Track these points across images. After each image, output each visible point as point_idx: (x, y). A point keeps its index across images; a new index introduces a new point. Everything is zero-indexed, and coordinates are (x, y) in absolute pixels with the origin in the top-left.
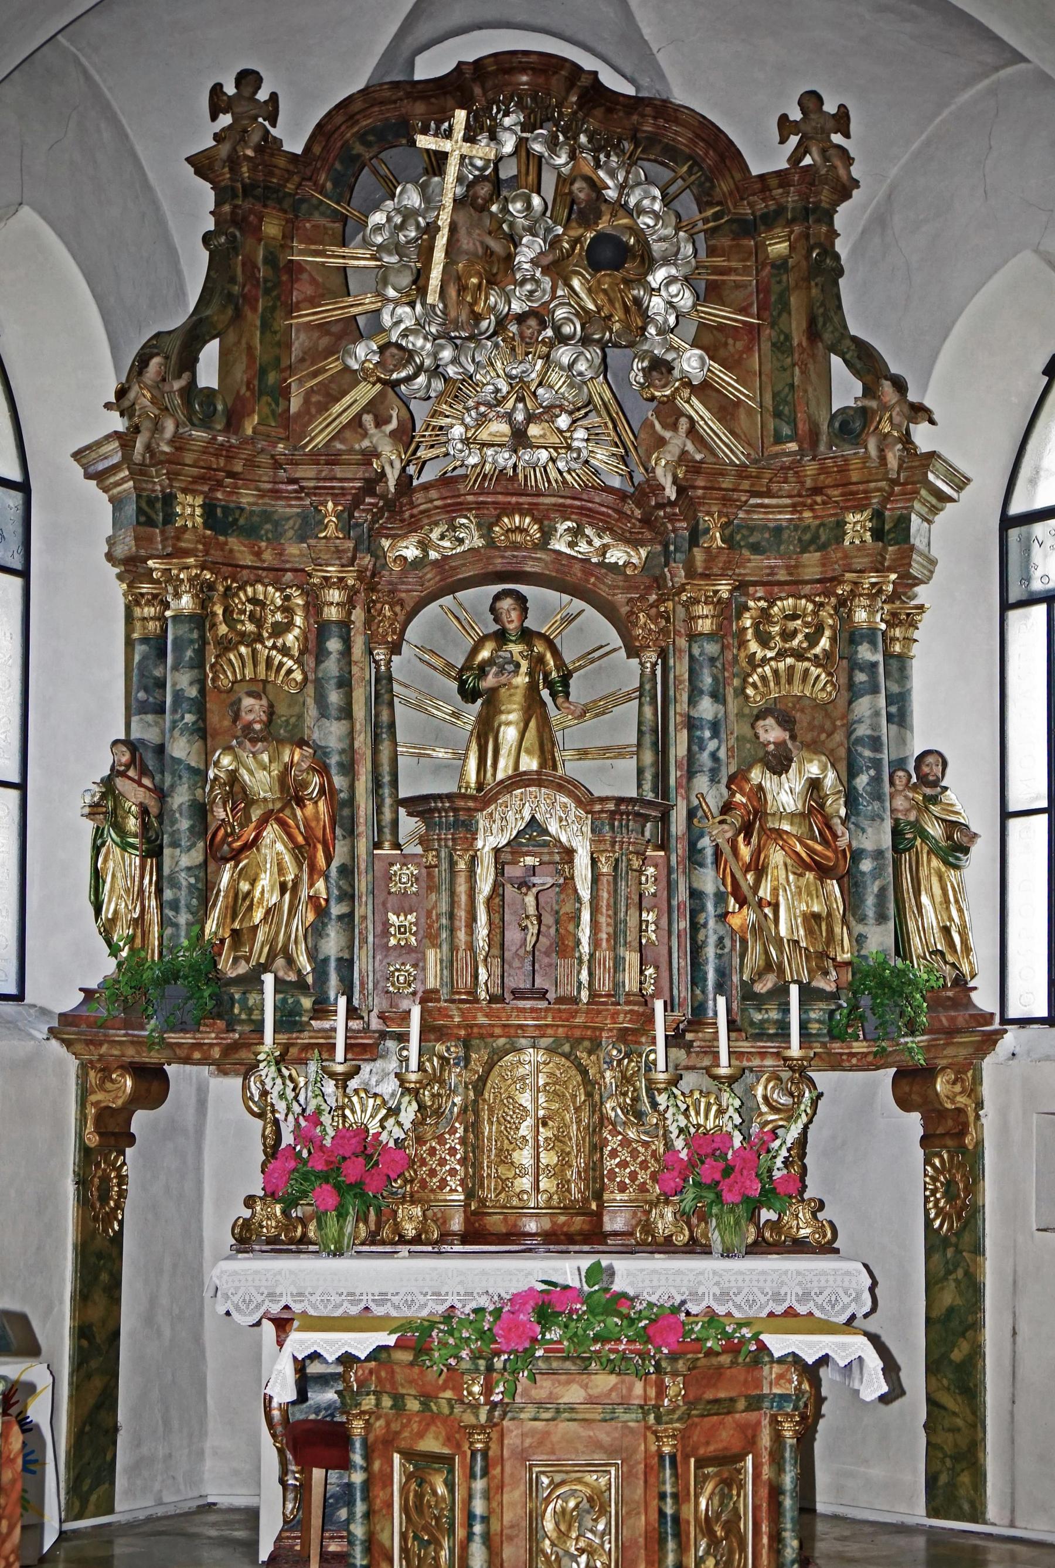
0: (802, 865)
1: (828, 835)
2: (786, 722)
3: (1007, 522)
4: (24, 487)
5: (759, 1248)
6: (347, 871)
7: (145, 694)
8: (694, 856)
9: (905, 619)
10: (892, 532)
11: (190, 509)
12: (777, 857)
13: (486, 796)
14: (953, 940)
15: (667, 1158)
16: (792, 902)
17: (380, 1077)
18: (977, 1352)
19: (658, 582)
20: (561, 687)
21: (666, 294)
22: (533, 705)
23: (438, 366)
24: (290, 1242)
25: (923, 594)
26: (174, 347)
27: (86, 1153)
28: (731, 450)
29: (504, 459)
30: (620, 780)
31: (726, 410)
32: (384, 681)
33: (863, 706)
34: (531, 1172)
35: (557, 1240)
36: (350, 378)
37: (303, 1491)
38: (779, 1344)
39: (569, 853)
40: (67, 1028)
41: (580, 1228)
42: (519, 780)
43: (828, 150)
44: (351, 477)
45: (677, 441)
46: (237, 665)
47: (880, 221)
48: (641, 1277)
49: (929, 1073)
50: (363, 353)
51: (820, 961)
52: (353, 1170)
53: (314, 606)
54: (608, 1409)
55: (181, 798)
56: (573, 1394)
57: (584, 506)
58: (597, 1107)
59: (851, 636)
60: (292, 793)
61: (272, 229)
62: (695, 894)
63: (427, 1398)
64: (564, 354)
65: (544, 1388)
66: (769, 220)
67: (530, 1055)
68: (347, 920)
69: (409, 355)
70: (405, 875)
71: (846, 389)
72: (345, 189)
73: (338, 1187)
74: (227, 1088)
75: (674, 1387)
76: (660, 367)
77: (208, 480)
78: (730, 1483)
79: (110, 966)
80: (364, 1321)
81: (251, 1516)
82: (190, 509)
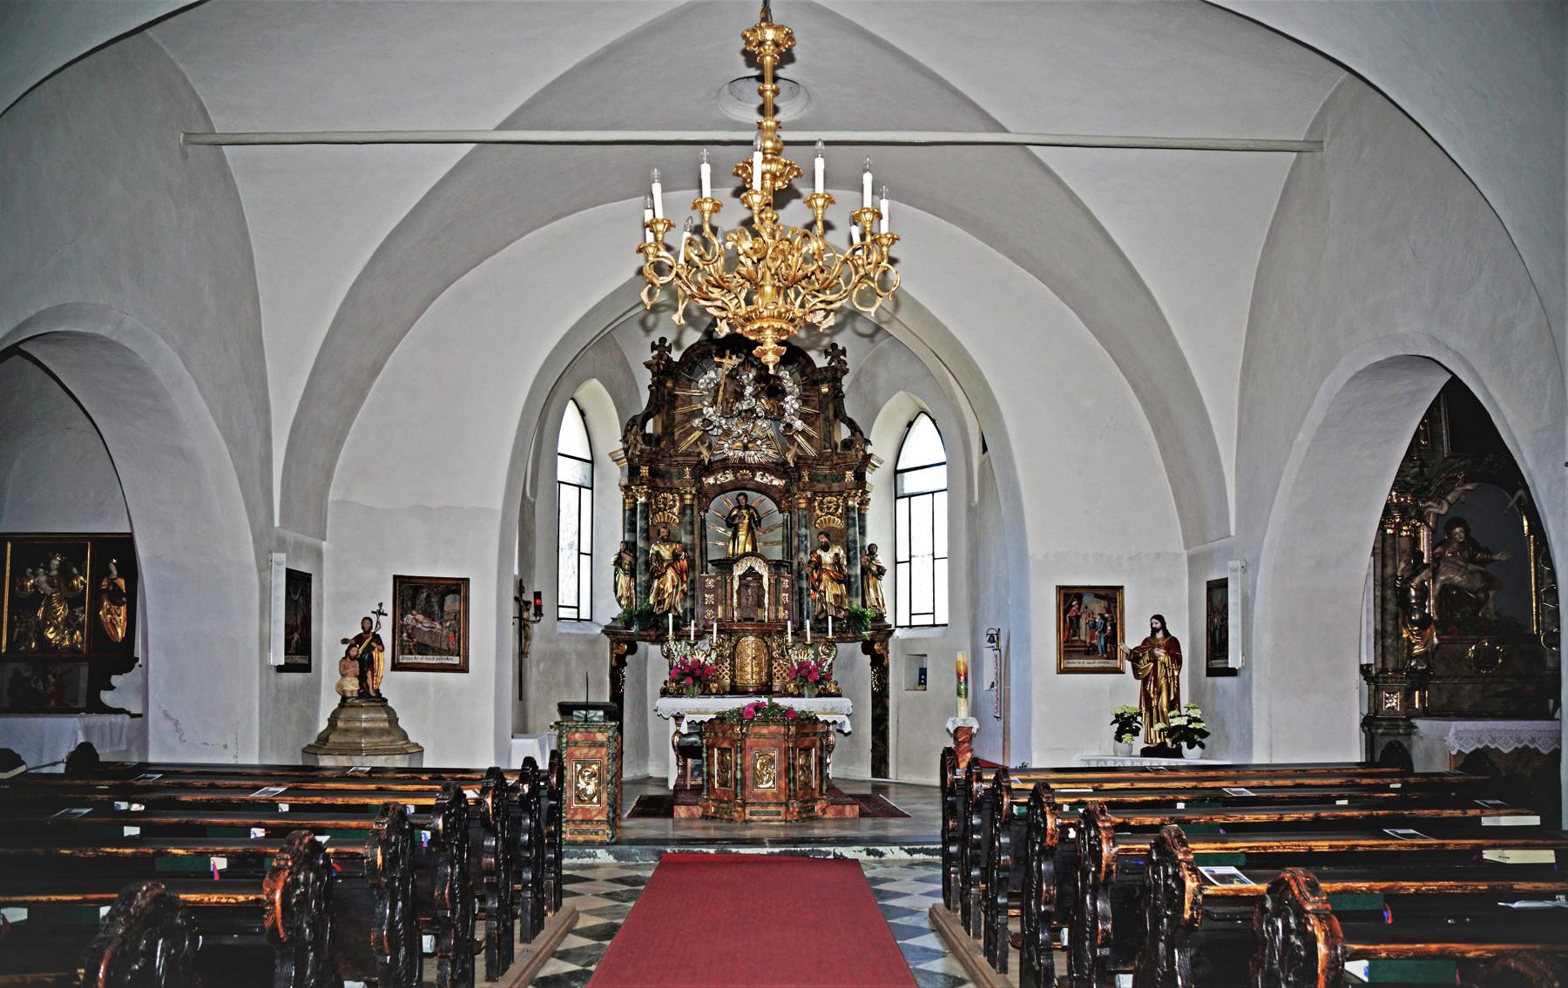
0: (833, 580)
1: (841, 571)
2: (827, 536)
3: (897, 472)
4: (592, 462)
5: (819, 695)
6: (693, 582)
7: (630, 526)
8: (800, 577)
9: (864, 503)
10: (860, 478)
11: (645, 471)
12: (824, 577)
13: (737, 559)
14: (880, 605)
15: (792, 669)
16: (831, 590)
17: (704, 645)
18: (887, 727)
19: (788, 491)
20: (758, 523)
21: (791, 403)
22: (750, 529)
23: (883, 789)
24: (679, 694)
25: (870, 496)
26: (639, 421)
27: (612, 667)
28: (811, 452)
29: (740, 454)
30: (777, 553)
31: (809, 439)
32: (703, 522)
33: (851, 531)
34: (750, 675)
35: (758, 693)
36: (693, 429)
37: (684, 767)
38: (821, 718)
39: (761, 577)
40: (608, 631)
41: (765, 689)
42: (746, 554)
43: (840, 361)
44: (694, 460)
45: (794, 450)
46: (659, 517)
47: (857, 379)
48: (783, 702)
49: (872, 642)
50: (697, 422)
51: (838, 608)
52: (698, 672)
53: (682, 500)
54: (774, 735)
55: (641, 560)
56: (765, 731)
57: (764, 468)
58: (770, 653)
59: (848, 509)
60: (676, 557)
61: (669, 384)
62: (801, 589)
63: (724, 733)
64: (759, 422)
65: (757, 729)
66: (823, 381)
67: (751, 638)
68: (693, 596)
69: (711, 423)
70: (710, 583)
71: (844, 432)
72: (691, 372)
73: (692, 679)
74: (655, 650)
75: (793, 729)
76: (789, 426)
77: (650, 462)
78: (808, 756)
79: (620, 611)
80: (706, 713)
81: (666, 780)
82: (645, 471)
